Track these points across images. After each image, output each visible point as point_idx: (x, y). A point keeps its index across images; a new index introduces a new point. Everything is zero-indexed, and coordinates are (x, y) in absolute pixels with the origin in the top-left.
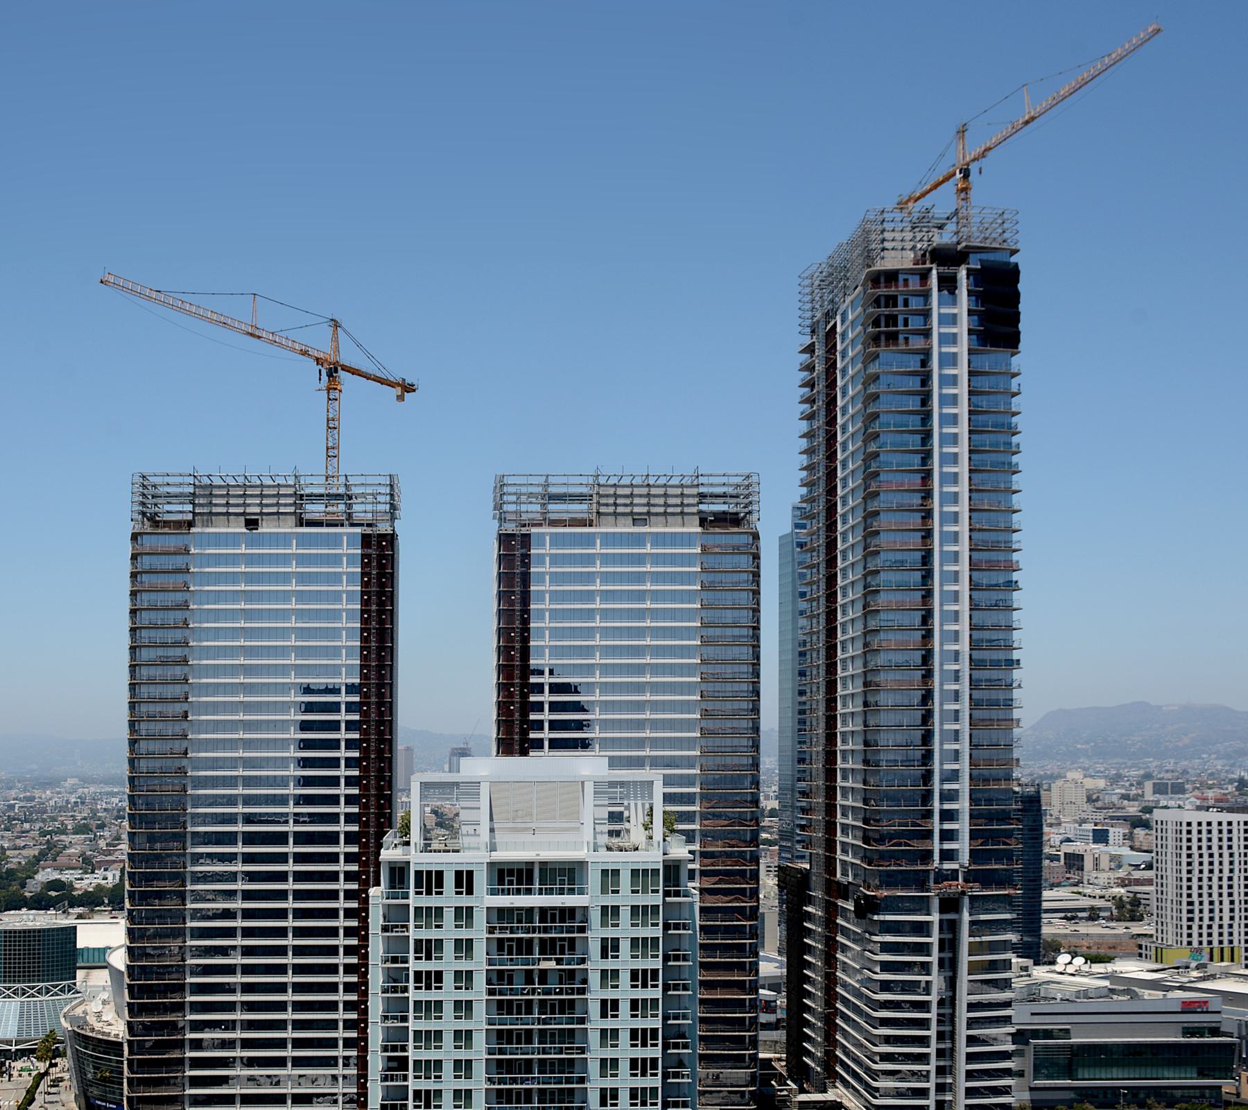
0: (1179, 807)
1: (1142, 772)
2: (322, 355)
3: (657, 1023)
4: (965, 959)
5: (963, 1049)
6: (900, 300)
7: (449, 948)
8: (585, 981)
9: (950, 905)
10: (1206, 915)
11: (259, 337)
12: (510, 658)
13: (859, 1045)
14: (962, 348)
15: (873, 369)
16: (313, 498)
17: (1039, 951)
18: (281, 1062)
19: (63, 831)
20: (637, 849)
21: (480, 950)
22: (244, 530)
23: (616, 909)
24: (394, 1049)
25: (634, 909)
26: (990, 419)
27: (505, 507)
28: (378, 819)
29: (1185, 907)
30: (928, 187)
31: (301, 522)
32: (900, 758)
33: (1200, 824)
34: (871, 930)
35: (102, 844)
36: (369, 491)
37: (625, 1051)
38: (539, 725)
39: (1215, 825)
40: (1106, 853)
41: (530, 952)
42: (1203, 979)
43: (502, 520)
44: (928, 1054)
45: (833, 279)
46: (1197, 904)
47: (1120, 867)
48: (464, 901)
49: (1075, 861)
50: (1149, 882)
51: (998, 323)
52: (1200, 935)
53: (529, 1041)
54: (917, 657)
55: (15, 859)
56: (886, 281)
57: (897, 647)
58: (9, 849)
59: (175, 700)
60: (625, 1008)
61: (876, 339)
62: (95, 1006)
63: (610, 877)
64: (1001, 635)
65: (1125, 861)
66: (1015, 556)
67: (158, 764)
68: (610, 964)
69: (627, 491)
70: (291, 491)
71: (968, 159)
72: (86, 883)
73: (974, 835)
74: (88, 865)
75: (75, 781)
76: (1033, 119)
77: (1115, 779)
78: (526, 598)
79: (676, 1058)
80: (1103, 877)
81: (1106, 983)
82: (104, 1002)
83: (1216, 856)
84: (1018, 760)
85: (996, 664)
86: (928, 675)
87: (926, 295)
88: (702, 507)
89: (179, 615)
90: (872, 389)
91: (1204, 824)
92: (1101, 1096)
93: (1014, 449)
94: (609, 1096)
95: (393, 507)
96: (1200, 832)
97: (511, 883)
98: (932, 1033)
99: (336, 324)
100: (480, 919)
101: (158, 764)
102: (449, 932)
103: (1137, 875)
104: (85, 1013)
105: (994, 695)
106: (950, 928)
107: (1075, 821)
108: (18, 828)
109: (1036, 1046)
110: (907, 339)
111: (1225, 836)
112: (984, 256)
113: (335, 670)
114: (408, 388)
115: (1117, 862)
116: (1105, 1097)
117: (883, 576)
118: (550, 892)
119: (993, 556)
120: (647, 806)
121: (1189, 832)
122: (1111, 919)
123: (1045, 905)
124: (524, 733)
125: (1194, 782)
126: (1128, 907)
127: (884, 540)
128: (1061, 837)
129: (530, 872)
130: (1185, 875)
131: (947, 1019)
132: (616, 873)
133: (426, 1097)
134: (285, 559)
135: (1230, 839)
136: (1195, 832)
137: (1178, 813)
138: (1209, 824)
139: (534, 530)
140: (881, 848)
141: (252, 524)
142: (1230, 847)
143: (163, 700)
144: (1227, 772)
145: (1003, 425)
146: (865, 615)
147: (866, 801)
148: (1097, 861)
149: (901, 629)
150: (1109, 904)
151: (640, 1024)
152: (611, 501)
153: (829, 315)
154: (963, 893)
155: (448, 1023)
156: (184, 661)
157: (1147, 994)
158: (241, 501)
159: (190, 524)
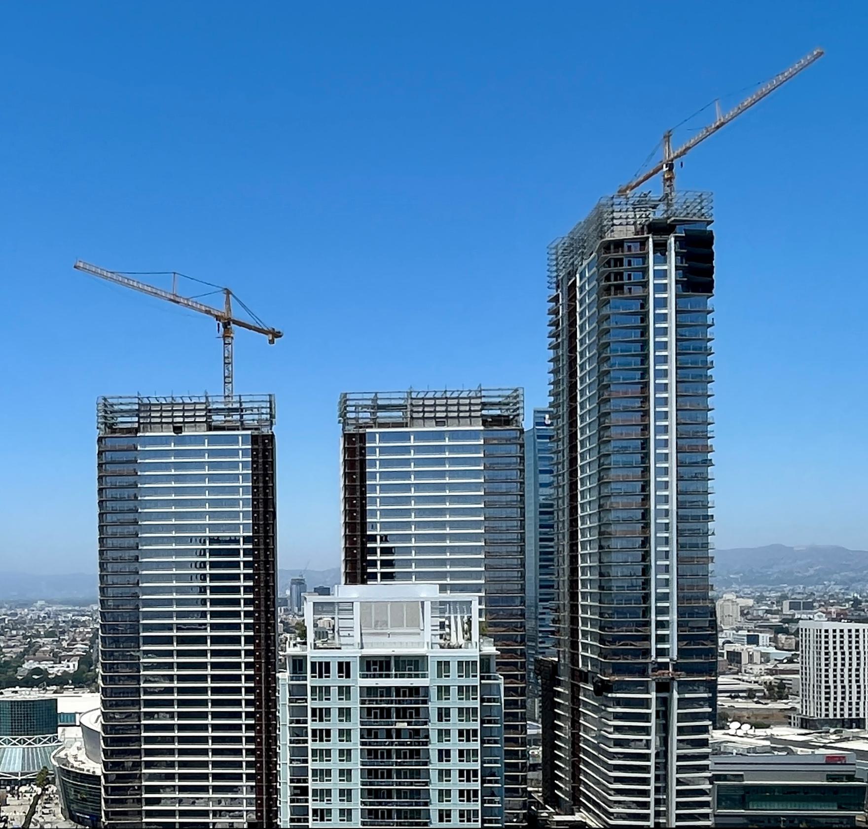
0: (810, 619)
1: (779, 594)
2: (220, 314)
3: (477, 766)
4: (675, 724)
5: (674, 788)
6: (625, 261)
7: (335, 713)
8: (427, 737)
9: (663, 687)
10: (839, 695)
11: (178, 302)
12: (352, 518)
13: (598, 783)
14: (671, 294)
15: (606, 311)
16: (218, 411)
17: (720, 720)
18: (205, 789)
19: (39, 636)
20: (460, 647)
21: (356, 715)
22: (173, 434)
23: (447, 688)
24: (299, 781)
25: (460, 688)
26: (692, 344)
27: (348, 415)
28: (266, 627)
29: (823, 690)
30: (641, 178)
31: (210, 428)
32: (626, 585)
33: (834, 631)
34: (605, 703)
35: (65, 644)
36: (256, 405)
37: (455, 784)
38: (373, 564)
39: (846, 632)
40: (757, 651)
41: (389, 717)
42: (837, 741)
43: (345, 424)
44: (649, 790)
45: (575, 247)
46: (832, 687)
47: (768, 661)
48: (344, 682)
49: (735, 657)
50: (796, 672)
51: (697, 276)
52: (835, 710)
53: (390, 776)
54: (639, 514)
55: (10, 654)
56: (615, 248)
57: (623, 506)
58: (4, 647)
59: (130, 548)
60: (454, 755)
61: (608, 290)
62: (72, 751)
63: (443, 666)
64: (700, 498)
65: (772, 657)
66: (710, 442)
67: (120, 591)
68: (444, 726)
69: (432, 402)
70: (203, 407)
71: (672, 156)
72: (56, 670)
73: (680, 638)
74: (57, 658)
75: (43, 602)
76: (722, 124)
77: (759, 600)
78: (363, 476)
79: (489, 790)
80: (757, 669)
81: (768, 743)
82: (79, 749)
83: (847, 653)
84: (712, 586)
85: (696, 518)
86: (647, 526)
87: (645, 257)
88: (484, 412)
89: (132, 491)
90: (605, 326)
91: (838, 631)
92: (766, 821)
93: (709, 365)
94: (444, 815)
95: (272, 416)
96: (834, 637)
97: (375, 670)
98: (652, 775)
99: (228, 293)
100: (355, 694)
101: (120, 591)
102: (334, 703)
103: (781, 667)
104: (66, 755)
105: (694, 540)
106: (664, 703)
107: (733, 629)
108: (9, 634)
109: (719, 785)
110: (630, 289)
111: (854, 639)
112: (687, 227)
113: (236, 527)
114: (277, 335)
115: (766, 658)
116: (769, 822)
117: (613, 458)
118: (402, 676)
119: (694, 442)
120: (465, 620)
121: (826, 637)
122: (764, 697)
123: (720, 687)
124: (364, 569)
125: (819, 601)
126: (776, 689)
127: (613, 432)
128: (723, 640)
129: (388, 663)
130: (823, 667)
131: (661, 766)
132: (447, 663)
133: (321, 814)
134: (200, 453)
135: (857, 642)
136: (831, 637)
137: (815, 622)
138: (842, 631)
139: (368, 430)
140: (613, 647)
141: (178, 429)
142: (857, 648)
143: (122, 549)
144: (843, 594)
145: (701, 348)
146: (599, 485)
147: (601, 615)
148: (751, 657)
149: (627, 494)
150: (762, 687)
151: (465, 766)
152: (421, 409)
153: (571, 274)
154: (673, 679)
155: (335, 764)
156: (135, 522)
157: (799, 751)
158: (170, 414)
159: (137, 430)
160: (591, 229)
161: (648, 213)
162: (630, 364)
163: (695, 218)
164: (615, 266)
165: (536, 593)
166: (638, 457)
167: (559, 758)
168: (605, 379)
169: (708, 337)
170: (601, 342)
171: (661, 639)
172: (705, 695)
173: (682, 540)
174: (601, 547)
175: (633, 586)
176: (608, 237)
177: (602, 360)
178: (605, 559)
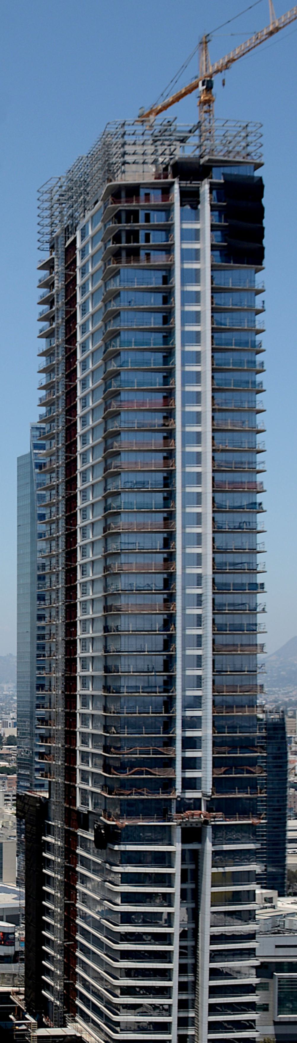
4: (207, 889)
9: (192, 834)
13: (99, 979)
15: (114, 285)
26: (234, 337)
30: (170, 99)
32: (141, 685)
34: (111, 860)
45: (73, 193)
51: (242, 241)
54: (159, 581)
57: (137, 572)
64: (245, 558)
71: (211, 70)
73: (217, 763)
76: (277, 29)
84: (262, 686)
85: (239, 588)
87: (168, 210)
90: (113, 306)
93: (258, 368)
105: (237, 620)
106: (193, 858)
109: (280, 979)
110: (148, 255)
112: (227, 170)
117: (124, 498)
119: (237, 477)
127: (125, 460)
140: (122, 776)
145: (246, 343)
146: (105, 538)
153: (68, 231)
154: (206, 823)
160: (96, 168)
161: (173, 148)
162: (148, 363)
163: (238, 159)
164: (128, 221)
165: (32, 697)
166: (159, 498)
167: (48, 942)
168: (114, 383)
169: (258, 327)
170: (108, 329)
171: (190, 764)
172: (251, 846)
173: (220, 619)
174: (106, 629)
175: (148, 687)
176: (120, 180)
177: (111, 356)
178: (112, 647)
